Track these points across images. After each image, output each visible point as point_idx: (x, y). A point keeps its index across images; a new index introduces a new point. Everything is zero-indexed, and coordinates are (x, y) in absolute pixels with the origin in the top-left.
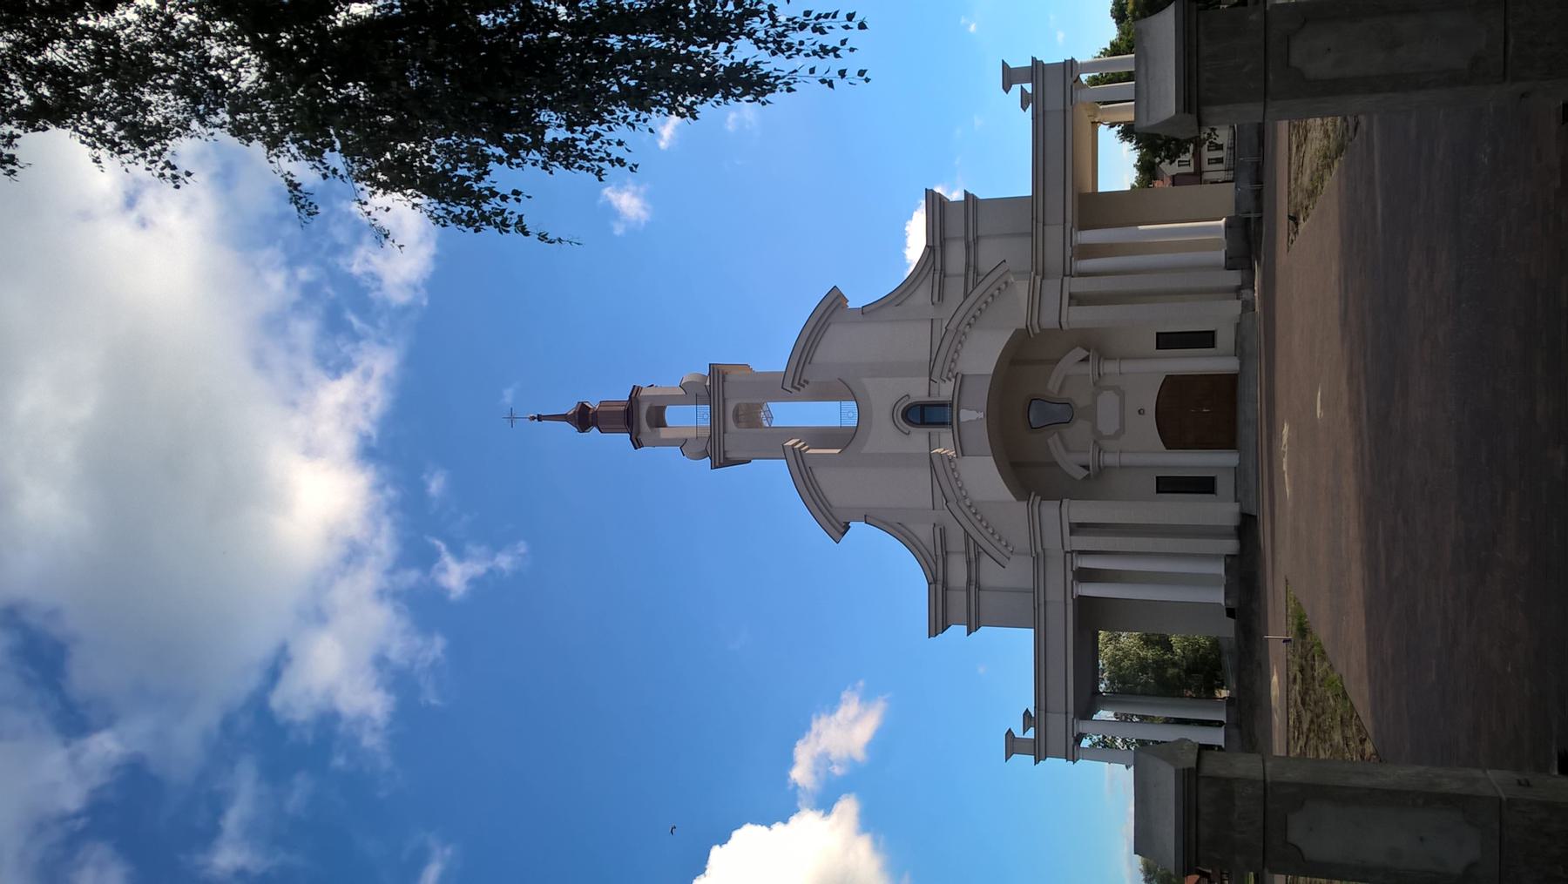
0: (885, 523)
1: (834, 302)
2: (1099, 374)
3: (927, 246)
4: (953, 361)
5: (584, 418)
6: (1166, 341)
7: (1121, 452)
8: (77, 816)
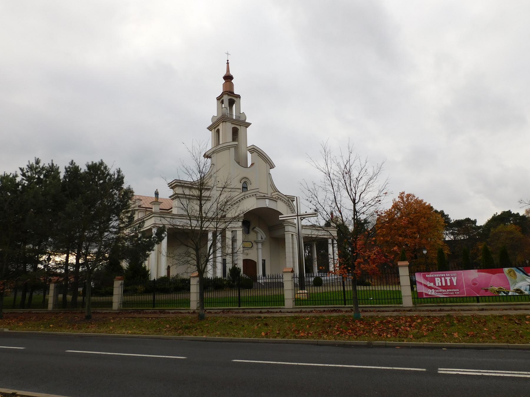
1: (272, 166)
2: (257, 243)
4: (281, 199)
5: (228, 78)
6: (264, 261)
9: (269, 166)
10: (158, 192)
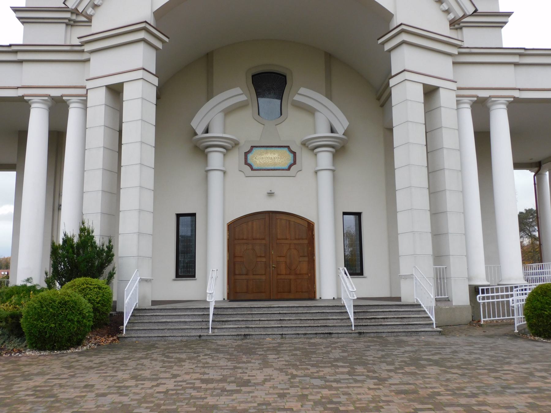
7: (225, 172)
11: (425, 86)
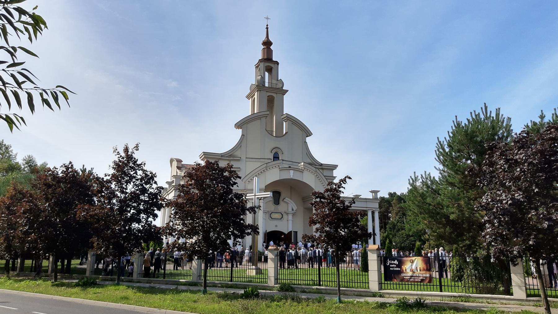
0: (241, 142)
3: (322, 164)
5: (267, 44)
8: (121, 285)
9: (305, 134)
10: (534, 122)
11: (512, 294)
